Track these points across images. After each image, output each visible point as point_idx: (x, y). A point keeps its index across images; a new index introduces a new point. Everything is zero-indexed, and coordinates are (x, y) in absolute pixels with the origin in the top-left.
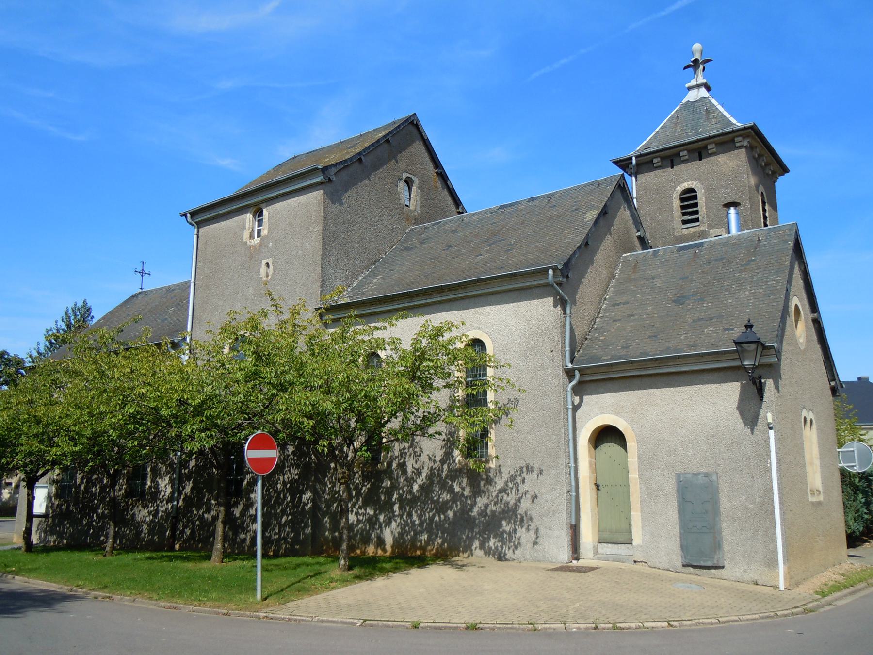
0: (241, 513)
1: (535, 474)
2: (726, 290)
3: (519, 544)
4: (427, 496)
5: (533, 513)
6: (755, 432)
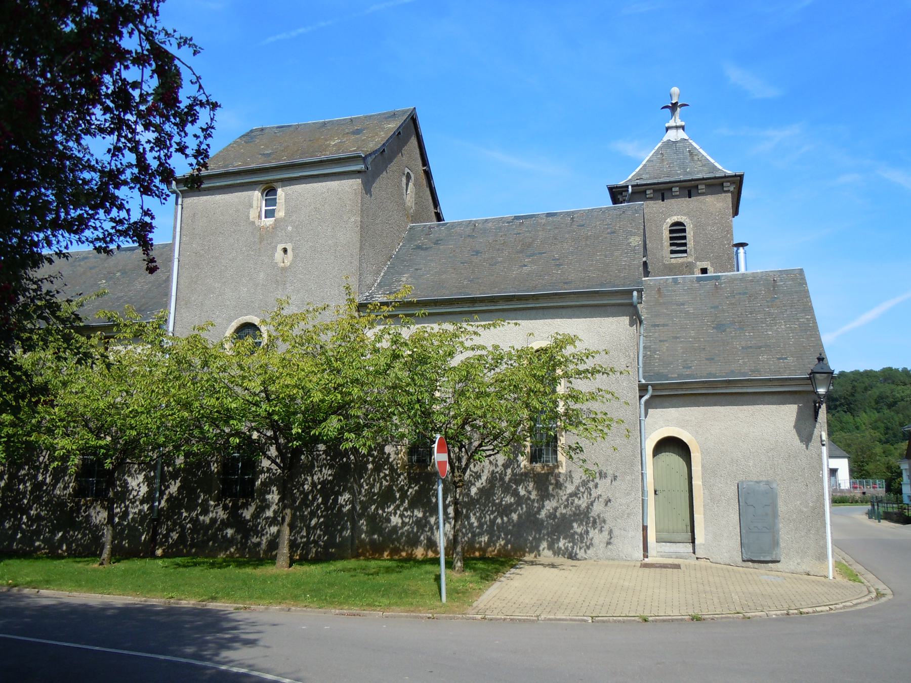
0: (252, 516)
1: (608, 480)
2: (762, 322)
3: (591, 544)
4: (488, 499)
5: (607, 516)
6: (810, 447)
